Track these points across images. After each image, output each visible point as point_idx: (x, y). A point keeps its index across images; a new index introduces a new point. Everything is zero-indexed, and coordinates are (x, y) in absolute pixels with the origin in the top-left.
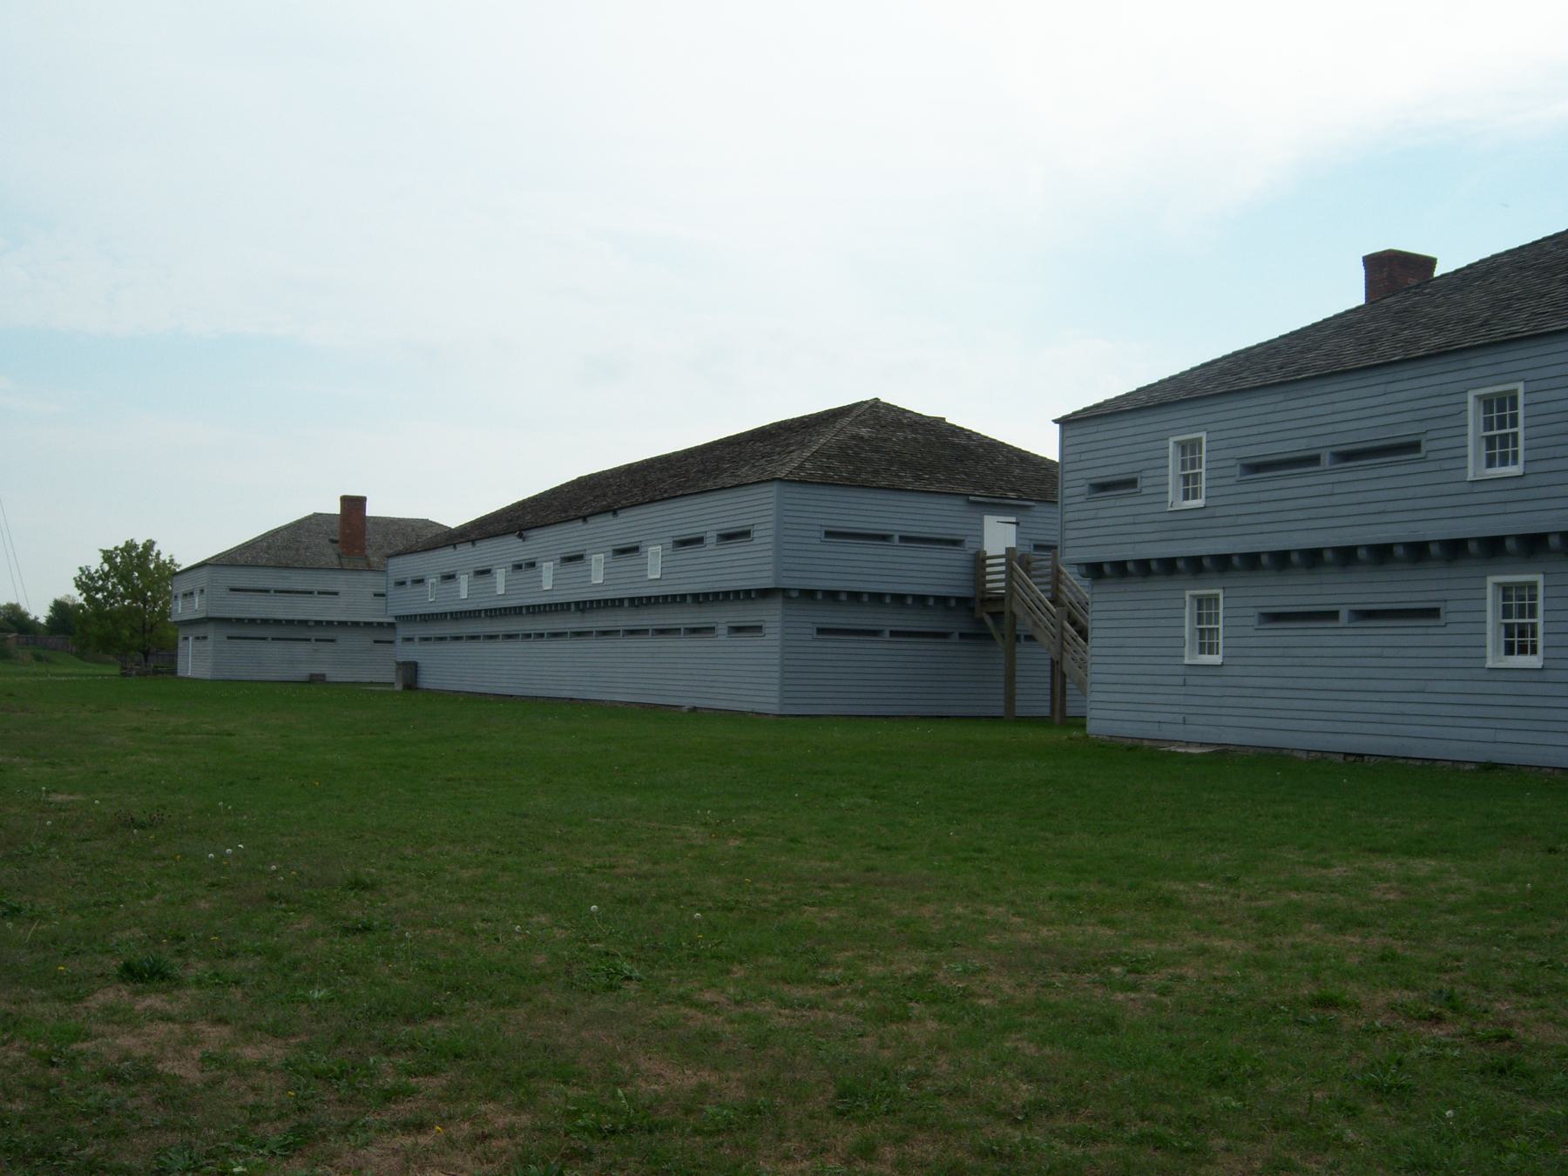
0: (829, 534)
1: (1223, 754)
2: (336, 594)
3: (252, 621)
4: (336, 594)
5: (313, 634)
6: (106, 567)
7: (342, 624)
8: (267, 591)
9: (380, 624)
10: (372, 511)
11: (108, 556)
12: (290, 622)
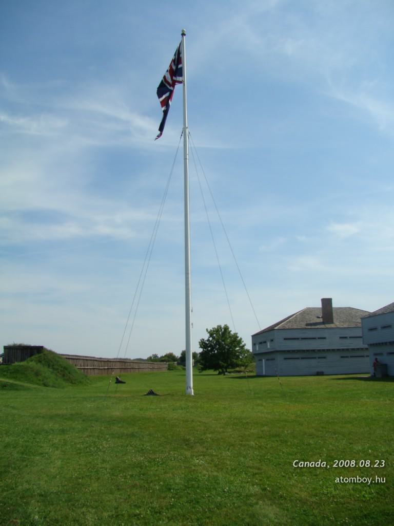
0: (285, 339)
1: (154, 360)
2: (325, 338)
3: (294, 351)
4: (325, 338)
5: (317, 355)
6: (211, 339)
7: (328, 350)
8: (298, 339)
9: (343, 350)
10: (335, 305)
11: (211, 334)
12: (308, 351)
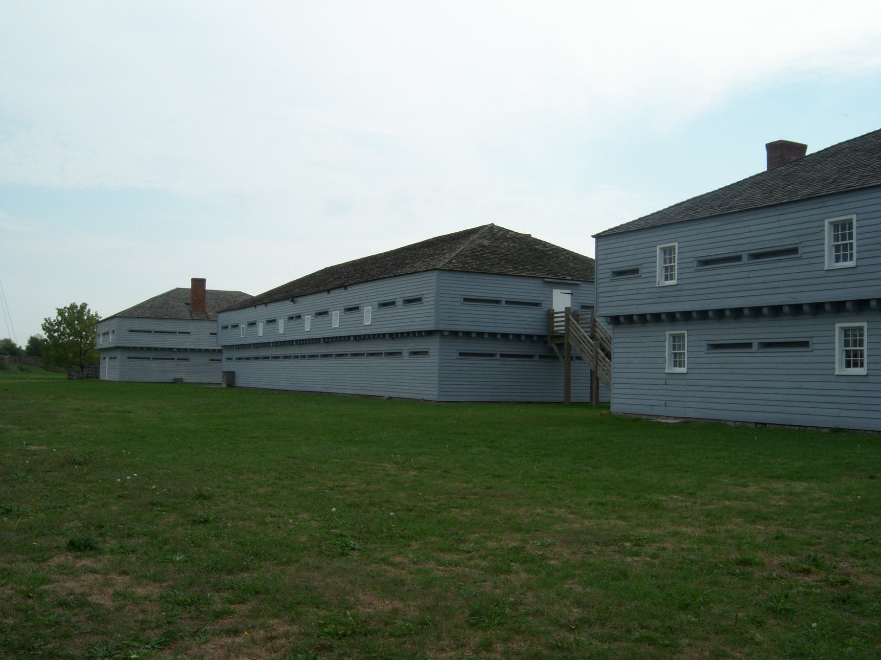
0: (466, 300)
1: (687, 423)
2: (189, 333)
3: (142, 349)
4: (189, 333)
5: (176, 356)
6: (60, 318)
7: (192, 350)
8: (150, 332)
9: (214, 350)
10: (209, 287)
11: (61, 312)
12: (163, 349)
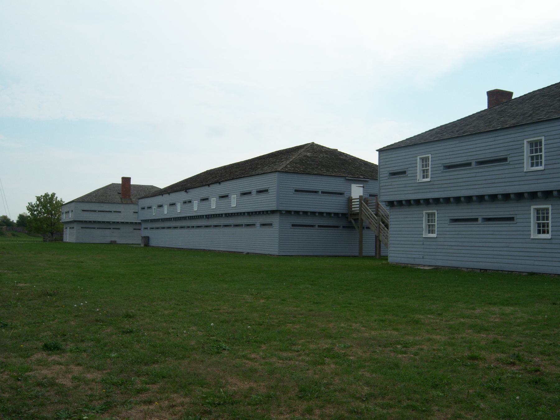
0: (296, 191)
1: (437, 269)
2: (120, 212)
3: (90, 222)
4: (120, 212)
5: (112, 227)
6: (38, 203)
7: (122, 223)
8: (95, 211)
9: (136, 223)
10: (133, 182)
11: (39, 199)
12: (104, 222)
